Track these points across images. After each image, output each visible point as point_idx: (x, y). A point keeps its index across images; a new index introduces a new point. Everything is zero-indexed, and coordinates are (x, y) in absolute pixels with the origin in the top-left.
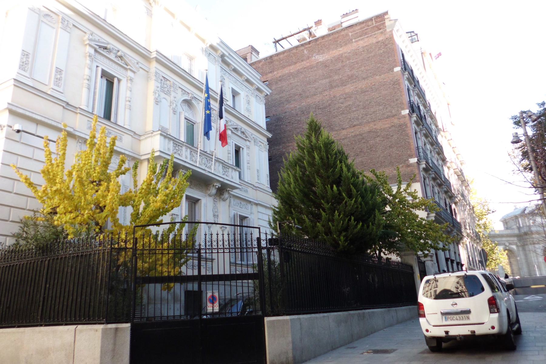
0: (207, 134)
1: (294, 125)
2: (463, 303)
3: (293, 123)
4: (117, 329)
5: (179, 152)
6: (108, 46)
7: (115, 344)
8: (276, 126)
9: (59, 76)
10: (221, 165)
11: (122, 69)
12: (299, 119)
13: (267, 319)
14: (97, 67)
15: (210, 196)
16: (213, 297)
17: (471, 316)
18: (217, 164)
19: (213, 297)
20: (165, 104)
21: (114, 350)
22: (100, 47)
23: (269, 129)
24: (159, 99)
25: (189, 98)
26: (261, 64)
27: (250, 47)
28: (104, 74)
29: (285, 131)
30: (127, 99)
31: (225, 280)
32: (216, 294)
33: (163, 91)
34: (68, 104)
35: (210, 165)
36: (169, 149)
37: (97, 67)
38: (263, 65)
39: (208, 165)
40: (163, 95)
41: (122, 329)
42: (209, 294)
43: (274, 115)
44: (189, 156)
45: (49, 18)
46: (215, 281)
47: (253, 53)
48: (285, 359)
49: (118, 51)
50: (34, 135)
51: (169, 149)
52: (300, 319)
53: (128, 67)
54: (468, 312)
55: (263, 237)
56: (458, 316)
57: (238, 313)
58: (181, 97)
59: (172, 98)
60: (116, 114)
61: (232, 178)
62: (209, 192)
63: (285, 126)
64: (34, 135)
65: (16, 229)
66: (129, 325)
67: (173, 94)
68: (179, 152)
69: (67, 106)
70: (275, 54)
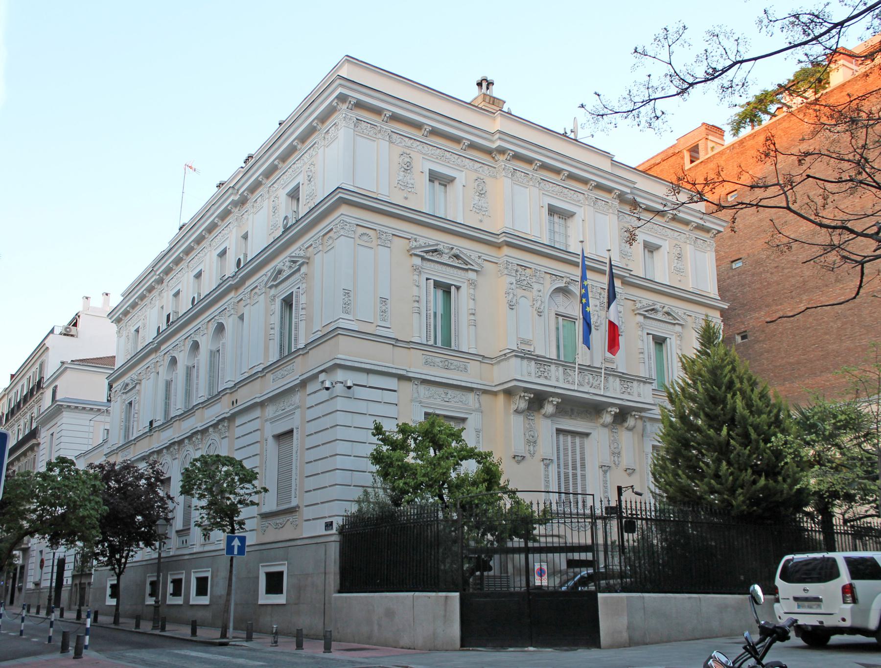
0: (587, 342)
1: (786, 271)
2: (813, 589)
3: (783, 269)
4: (446, 597)
5: (546, 374)
6: (440, 247)
7: (445, 611)
8: (753, 275)
9: (384, 308)
10: (618, 379)
11: (460, 272)
12: (794, 258)
13: (600, 595)
14: (427, 279)
15: (604, 426)
16: (541, 569)
17: (823, 605)
18: (611, 379)
19: (541, 569)
20: (525, 304)
21: (445, 616)
22: (427, 252)
23: (723, 298)
24: (514, 301)
25: (563, 285)
26: (724, 158)
27: (704, 128)
28: (437, 285)
29: (769, 284)
30: (471, 312)
31: (580, 552)
32: (545, 567)
33: (521, 287)
34: (397, 340)
35: (598, 382)
36: (529, 374)
37: (427, 279)
38: (727, 160)
39: (595, 383)
40: (520, 292)
41: (454, 597)
42: (537, 566)
43: (749, 255)
44: (561, 377)
45: (365, 238)
46: (832, 522)
47: (710, 137)
48: (627, 638)
49: (452, 248)
50: (365, 386)
51: (529, 374)
52: (643, 597)
53: (469, 266)
54: (817, 600)
55: (598, 505)
56: (806, 603)
57: (521, 587)
58: (549, 286)
59: (535, 293)
60: (457, 336)
61: (639, 395)
62: (601, 421)
63: (769, 275)
64: (365, 386)
65: (358, 493)
66: (458, 594)
67: (536, 286)
68: (546, 374)
69: (396, 342)
70: (750, 136)
